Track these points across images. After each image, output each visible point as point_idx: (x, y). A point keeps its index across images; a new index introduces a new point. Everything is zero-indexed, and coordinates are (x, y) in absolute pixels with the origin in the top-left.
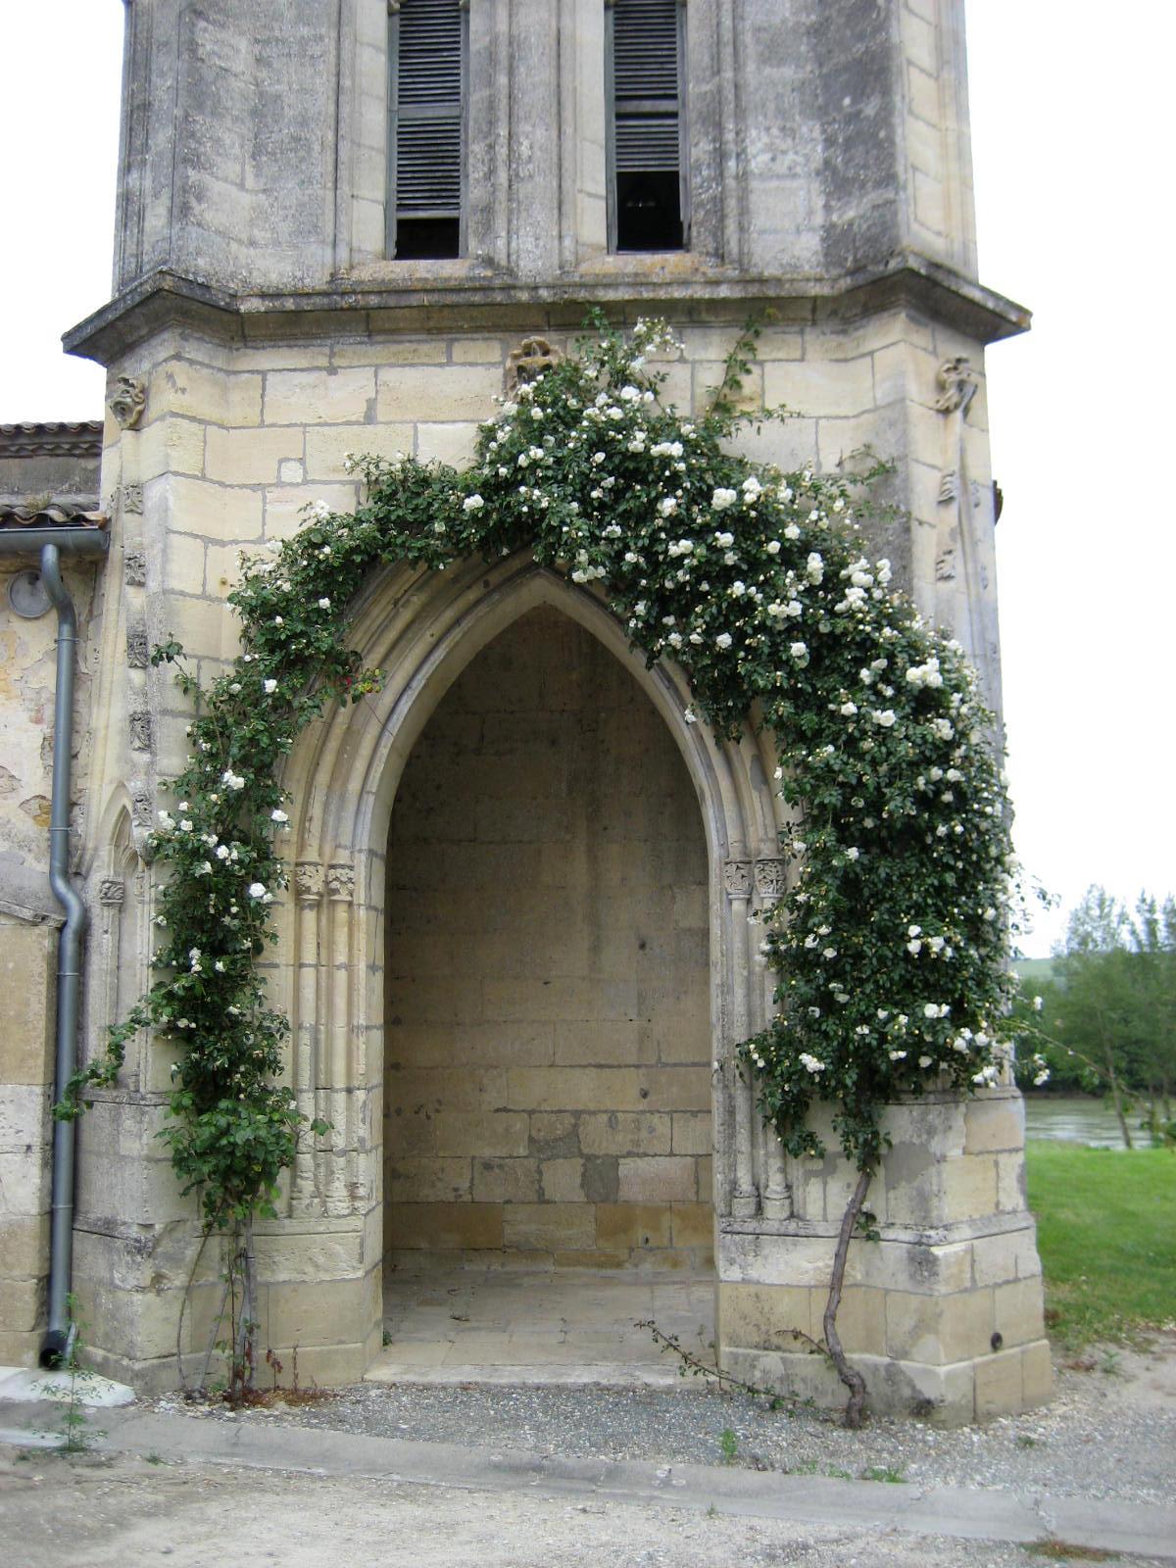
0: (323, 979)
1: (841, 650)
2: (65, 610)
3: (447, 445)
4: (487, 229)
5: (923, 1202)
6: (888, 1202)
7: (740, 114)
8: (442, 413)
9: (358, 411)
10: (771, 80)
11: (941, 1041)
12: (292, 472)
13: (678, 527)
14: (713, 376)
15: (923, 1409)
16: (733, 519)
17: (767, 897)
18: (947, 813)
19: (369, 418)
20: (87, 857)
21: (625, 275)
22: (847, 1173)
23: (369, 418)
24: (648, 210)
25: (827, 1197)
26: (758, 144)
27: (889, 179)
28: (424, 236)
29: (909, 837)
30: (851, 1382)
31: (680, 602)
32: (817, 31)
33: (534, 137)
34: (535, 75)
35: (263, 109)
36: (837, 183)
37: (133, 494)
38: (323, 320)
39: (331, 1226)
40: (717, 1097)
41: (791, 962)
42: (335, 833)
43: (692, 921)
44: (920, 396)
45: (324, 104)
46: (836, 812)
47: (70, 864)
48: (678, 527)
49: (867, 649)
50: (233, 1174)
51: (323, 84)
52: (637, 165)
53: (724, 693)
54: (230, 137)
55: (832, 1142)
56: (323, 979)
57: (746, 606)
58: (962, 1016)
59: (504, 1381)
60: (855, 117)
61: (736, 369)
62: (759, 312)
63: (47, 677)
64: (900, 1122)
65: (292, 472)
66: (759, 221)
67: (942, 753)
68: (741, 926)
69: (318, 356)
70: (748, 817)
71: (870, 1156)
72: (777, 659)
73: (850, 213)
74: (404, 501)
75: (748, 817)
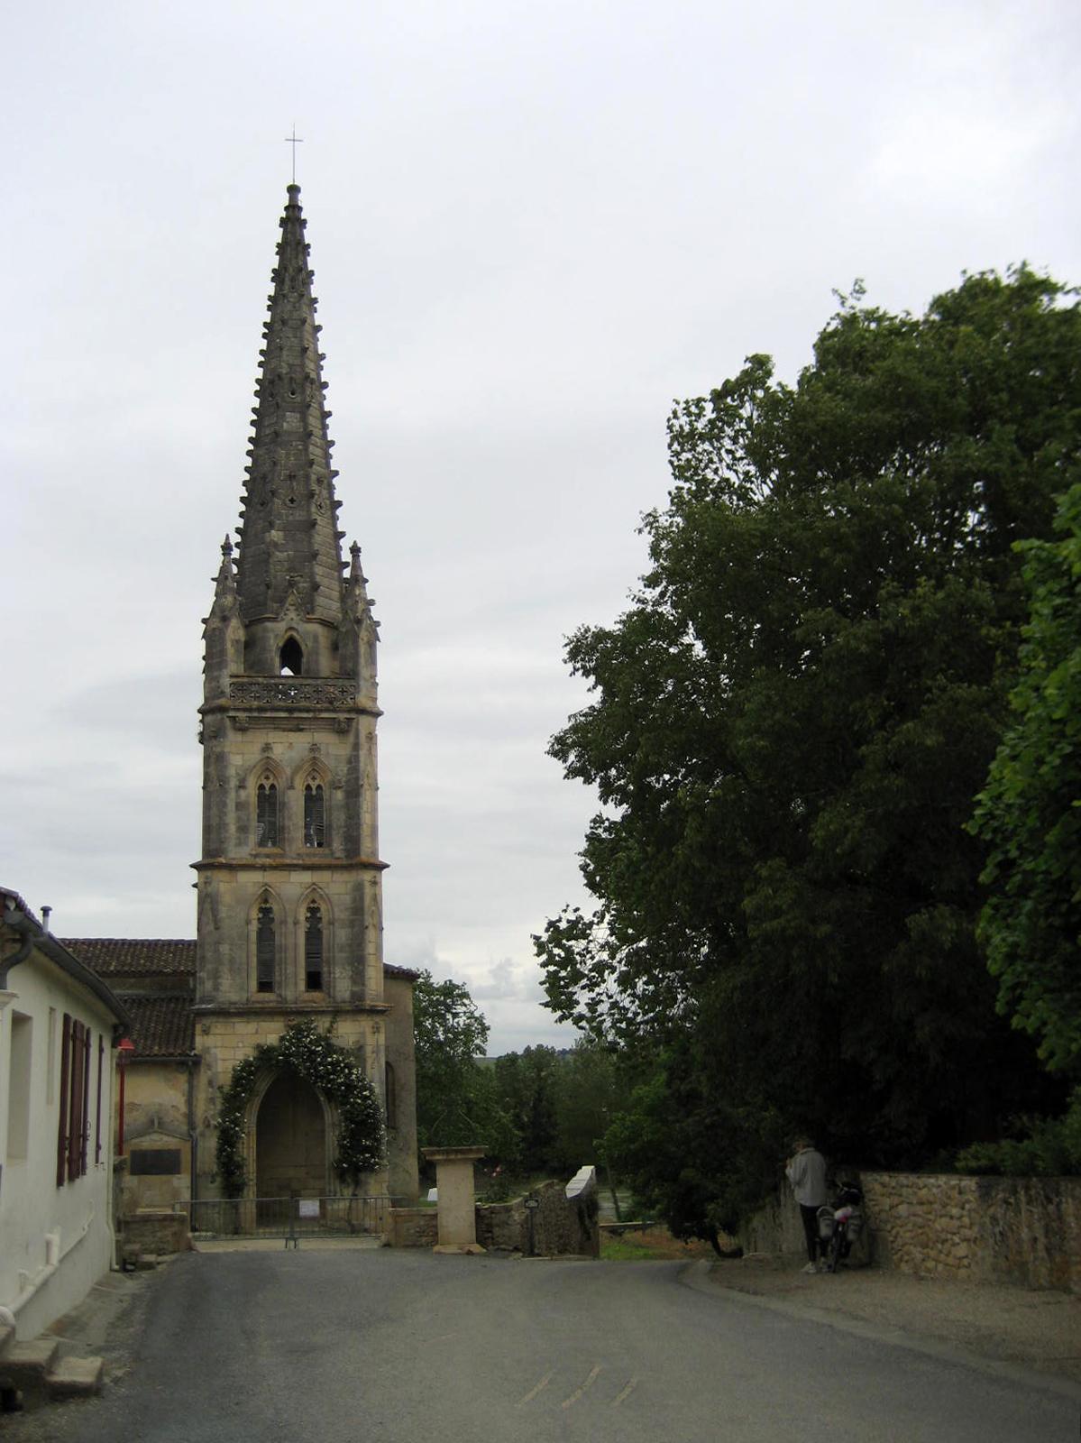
0: (248, 1149)
1: (350, 1087)
2: (191, 1074)
3: (272, 1039)
4: (280, 987)
5: (366, 1193)
6: (360, 1193)
7: (334, 964)
8: (271, 1033)
9: (254, 1031)
10: (341, 956)
11: (613, 1080)
12: (240, 1045)
13: (320, 1064)
14: (327, 1025)
15: (366, 1230)
16: (330, 1064)
17: (337, 1133)
18: (370, 1118)
19: (257, 1033)
20: (894, 1338)
21: (284, 819)
22: (352, 1186)
23: (257, 1033)
24: (314, 981)
25: (348, 1192)
26: (338, 972)
27: (364, 985)
28: (265, 986)
29: (363, 1122)
30: (353, 1226)
31: (322, 1077)
32: (350, 946)
33: (290, 969)
34: (290, 954)
35: (232, 961)
36: (354, 982)
37: (207, 1050)
38: (248, 1012)
39: (249, 1201)
40: (327, 1173)
41: (342, 1146)
42: (250, 1120)
43: (223, 884)
44: (368, 1030)
45: (244, 960)
46: (349, 1117)
47: (192, 1125)
48: (320, 1064)
49: (356, 1087)
50: (232, 1188)
51: (244, 955)
52: (312, 970)
53: (329, 1094)
54: (225, 969)
55: (349, 1180)
56: (248, 1149)
57: (334, 1079)
58: (373, 1157)
59: (413, 1078)
60: (357, 968)
61: (332, 1023)
62: (337, 1013)
63: (186, 1086)
64: (362, 1176)
65: (240, 1045)
66: (338, 989)
67: (370, 1106)
68: (332, 1139)
69: (245, 1020)
70: (332, 1116)
71: (357, 1183)
72: (339, 1089)
73: (355, 989)
74: (265, 1053)
75: (332, 1116)
